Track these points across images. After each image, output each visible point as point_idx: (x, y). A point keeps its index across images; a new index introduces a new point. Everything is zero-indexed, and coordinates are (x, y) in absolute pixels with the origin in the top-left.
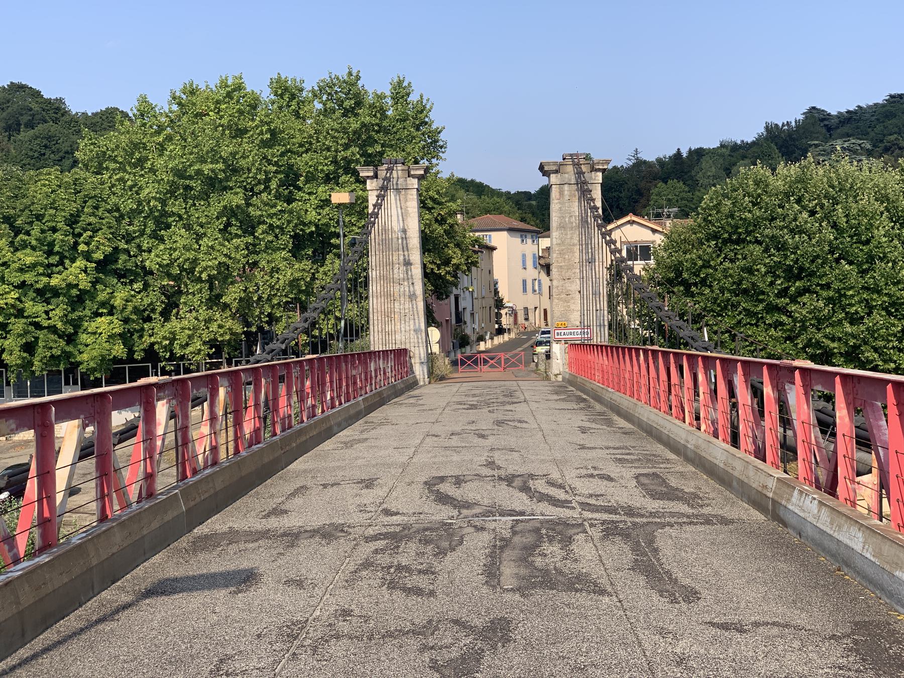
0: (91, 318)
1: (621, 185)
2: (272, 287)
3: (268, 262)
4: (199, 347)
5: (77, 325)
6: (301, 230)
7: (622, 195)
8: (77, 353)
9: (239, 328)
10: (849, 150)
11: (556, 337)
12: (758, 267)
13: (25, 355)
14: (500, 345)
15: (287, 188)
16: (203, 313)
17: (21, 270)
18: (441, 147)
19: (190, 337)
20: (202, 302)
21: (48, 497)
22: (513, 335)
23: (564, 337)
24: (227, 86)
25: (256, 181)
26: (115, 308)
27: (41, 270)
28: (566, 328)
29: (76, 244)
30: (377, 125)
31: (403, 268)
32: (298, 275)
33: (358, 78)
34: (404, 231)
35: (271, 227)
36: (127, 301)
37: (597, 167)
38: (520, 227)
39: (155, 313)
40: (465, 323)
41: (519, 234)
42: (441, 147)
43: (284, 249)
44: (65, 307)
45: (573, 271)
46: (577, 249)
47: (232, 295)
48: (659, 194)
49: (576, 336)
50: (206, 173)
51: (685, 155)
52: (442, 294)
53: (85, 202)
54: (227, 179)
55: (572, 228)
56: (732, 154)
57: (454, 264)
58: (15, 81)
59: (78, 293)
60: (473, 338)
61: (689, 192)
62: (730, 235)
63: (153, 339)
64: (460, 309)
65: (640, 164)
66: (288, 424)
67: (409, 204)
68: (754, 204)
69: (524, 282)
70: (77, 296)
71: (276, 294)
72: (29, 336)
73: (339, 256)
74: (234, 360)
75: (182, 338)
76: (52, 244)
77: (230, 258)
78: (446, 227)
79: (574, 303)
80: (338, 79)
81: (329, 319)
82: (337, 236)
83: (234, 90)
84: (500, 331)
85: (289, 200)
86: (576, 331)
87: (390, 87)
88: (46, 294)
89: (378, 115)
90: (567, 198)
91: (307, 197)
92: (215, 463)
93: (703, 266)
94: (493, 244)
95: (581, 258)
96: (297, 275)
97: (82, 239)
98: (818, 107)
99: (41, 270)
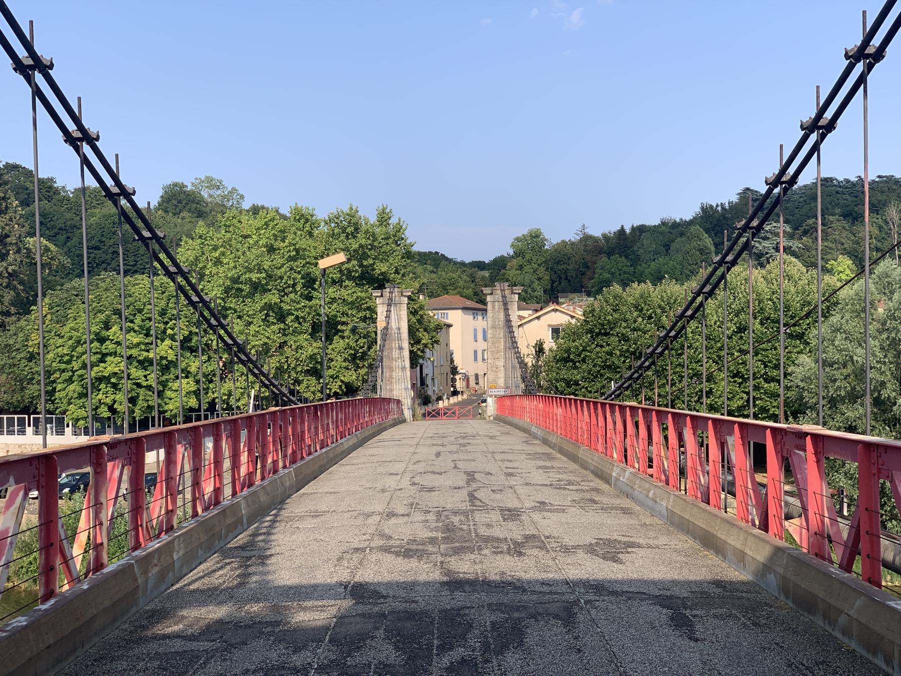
0: (174, 380)
1: (569, 259)
2: (297, 359)
3: (295, 341)
5: (164, 384)
6: (317, 319)
7: (570, 267)
8: (163, 404)
10: (771, 233)
13: (130, 405)
14: (455, 404)
15: (307, 290)
17: (128, 347)
19: (242, 394)
21: (218, 475)
22: (465, 397)
26: (190, 373)
27: (143, 347)
28: (495, 388)
30: (370, 244)
31: (398, 351)
32: (316, 351)
34: (399, 329)
35: (297, 318)
36: (199, 368)
39: (215, 377)
40: (427, 386)
41: (471, 312)
43: (305, 333)
46: (502, 341)
48: (602, 268)
51: (628, 231)
53: (169, 300)
54: (267, 284)
56: (671, 231)
57: (423, 344)
58: (11, 162)
60: (434, 398)
61: (631, 266)
62: (600, 330)
63: (216, 395)
65: (586, 238)
66: (249, 482)
67: (402, 312)
68: (614, 311)
69: (476, 352)
70: (166, 365)
72: (133, 392)
73: (343, 338)
76: (149, 329)
78: (418, 317)
80: (342, 212)
81: (336, 382)
82: (344, 323)
83: (270, 221)
84: (455, 393)
85: (310, 298)
87: (377, 212)
88: (145, 364)
89: (371, 238)
92: (170, 529)
93: (583, 350)
94: (449, 321)
95: (505, 345)
97: (169, 325)
98: (752, 188)
99: (143, 347)
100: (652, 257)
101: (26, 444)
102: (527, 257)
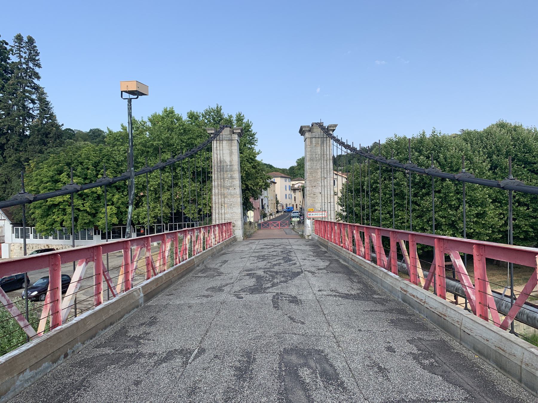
9: (167, 211)
11: (308, 216)
14: (278, 217)
16: (152, 205)
18: (256, 141)
22: (282, 213)
23: (312, 216)
24: (167, 111)
25: (176, 150)
28: (313, 212)
29: (97, 174)
33: (221, 110)
37: (330, 129)
40: (265, 209)
41: (284, 179)
42: (256, 141)
43: (188, 178)
44: (91, 202)
45: (317, 182)
47: (165, 197)
49: (319, 216)
50: (155, 145)
51: (335, 157)
52: (255, 197)
55: (317, 160)
59: (97, 196)
60: (268, 214)
62: (387, 168)
64: (263, 204)
67: (233, 148)
69: (286, 195)
75: (142, 215)
76: (86, 175)
77: (164, 181)
79: (317, 199)
80: (213, 109)
84: (278, 212)
86: (318, 213)
90: (314, 145)
91: (199, 156)
94: (275, 181)
96: (193, 189)
101: (30, 244)
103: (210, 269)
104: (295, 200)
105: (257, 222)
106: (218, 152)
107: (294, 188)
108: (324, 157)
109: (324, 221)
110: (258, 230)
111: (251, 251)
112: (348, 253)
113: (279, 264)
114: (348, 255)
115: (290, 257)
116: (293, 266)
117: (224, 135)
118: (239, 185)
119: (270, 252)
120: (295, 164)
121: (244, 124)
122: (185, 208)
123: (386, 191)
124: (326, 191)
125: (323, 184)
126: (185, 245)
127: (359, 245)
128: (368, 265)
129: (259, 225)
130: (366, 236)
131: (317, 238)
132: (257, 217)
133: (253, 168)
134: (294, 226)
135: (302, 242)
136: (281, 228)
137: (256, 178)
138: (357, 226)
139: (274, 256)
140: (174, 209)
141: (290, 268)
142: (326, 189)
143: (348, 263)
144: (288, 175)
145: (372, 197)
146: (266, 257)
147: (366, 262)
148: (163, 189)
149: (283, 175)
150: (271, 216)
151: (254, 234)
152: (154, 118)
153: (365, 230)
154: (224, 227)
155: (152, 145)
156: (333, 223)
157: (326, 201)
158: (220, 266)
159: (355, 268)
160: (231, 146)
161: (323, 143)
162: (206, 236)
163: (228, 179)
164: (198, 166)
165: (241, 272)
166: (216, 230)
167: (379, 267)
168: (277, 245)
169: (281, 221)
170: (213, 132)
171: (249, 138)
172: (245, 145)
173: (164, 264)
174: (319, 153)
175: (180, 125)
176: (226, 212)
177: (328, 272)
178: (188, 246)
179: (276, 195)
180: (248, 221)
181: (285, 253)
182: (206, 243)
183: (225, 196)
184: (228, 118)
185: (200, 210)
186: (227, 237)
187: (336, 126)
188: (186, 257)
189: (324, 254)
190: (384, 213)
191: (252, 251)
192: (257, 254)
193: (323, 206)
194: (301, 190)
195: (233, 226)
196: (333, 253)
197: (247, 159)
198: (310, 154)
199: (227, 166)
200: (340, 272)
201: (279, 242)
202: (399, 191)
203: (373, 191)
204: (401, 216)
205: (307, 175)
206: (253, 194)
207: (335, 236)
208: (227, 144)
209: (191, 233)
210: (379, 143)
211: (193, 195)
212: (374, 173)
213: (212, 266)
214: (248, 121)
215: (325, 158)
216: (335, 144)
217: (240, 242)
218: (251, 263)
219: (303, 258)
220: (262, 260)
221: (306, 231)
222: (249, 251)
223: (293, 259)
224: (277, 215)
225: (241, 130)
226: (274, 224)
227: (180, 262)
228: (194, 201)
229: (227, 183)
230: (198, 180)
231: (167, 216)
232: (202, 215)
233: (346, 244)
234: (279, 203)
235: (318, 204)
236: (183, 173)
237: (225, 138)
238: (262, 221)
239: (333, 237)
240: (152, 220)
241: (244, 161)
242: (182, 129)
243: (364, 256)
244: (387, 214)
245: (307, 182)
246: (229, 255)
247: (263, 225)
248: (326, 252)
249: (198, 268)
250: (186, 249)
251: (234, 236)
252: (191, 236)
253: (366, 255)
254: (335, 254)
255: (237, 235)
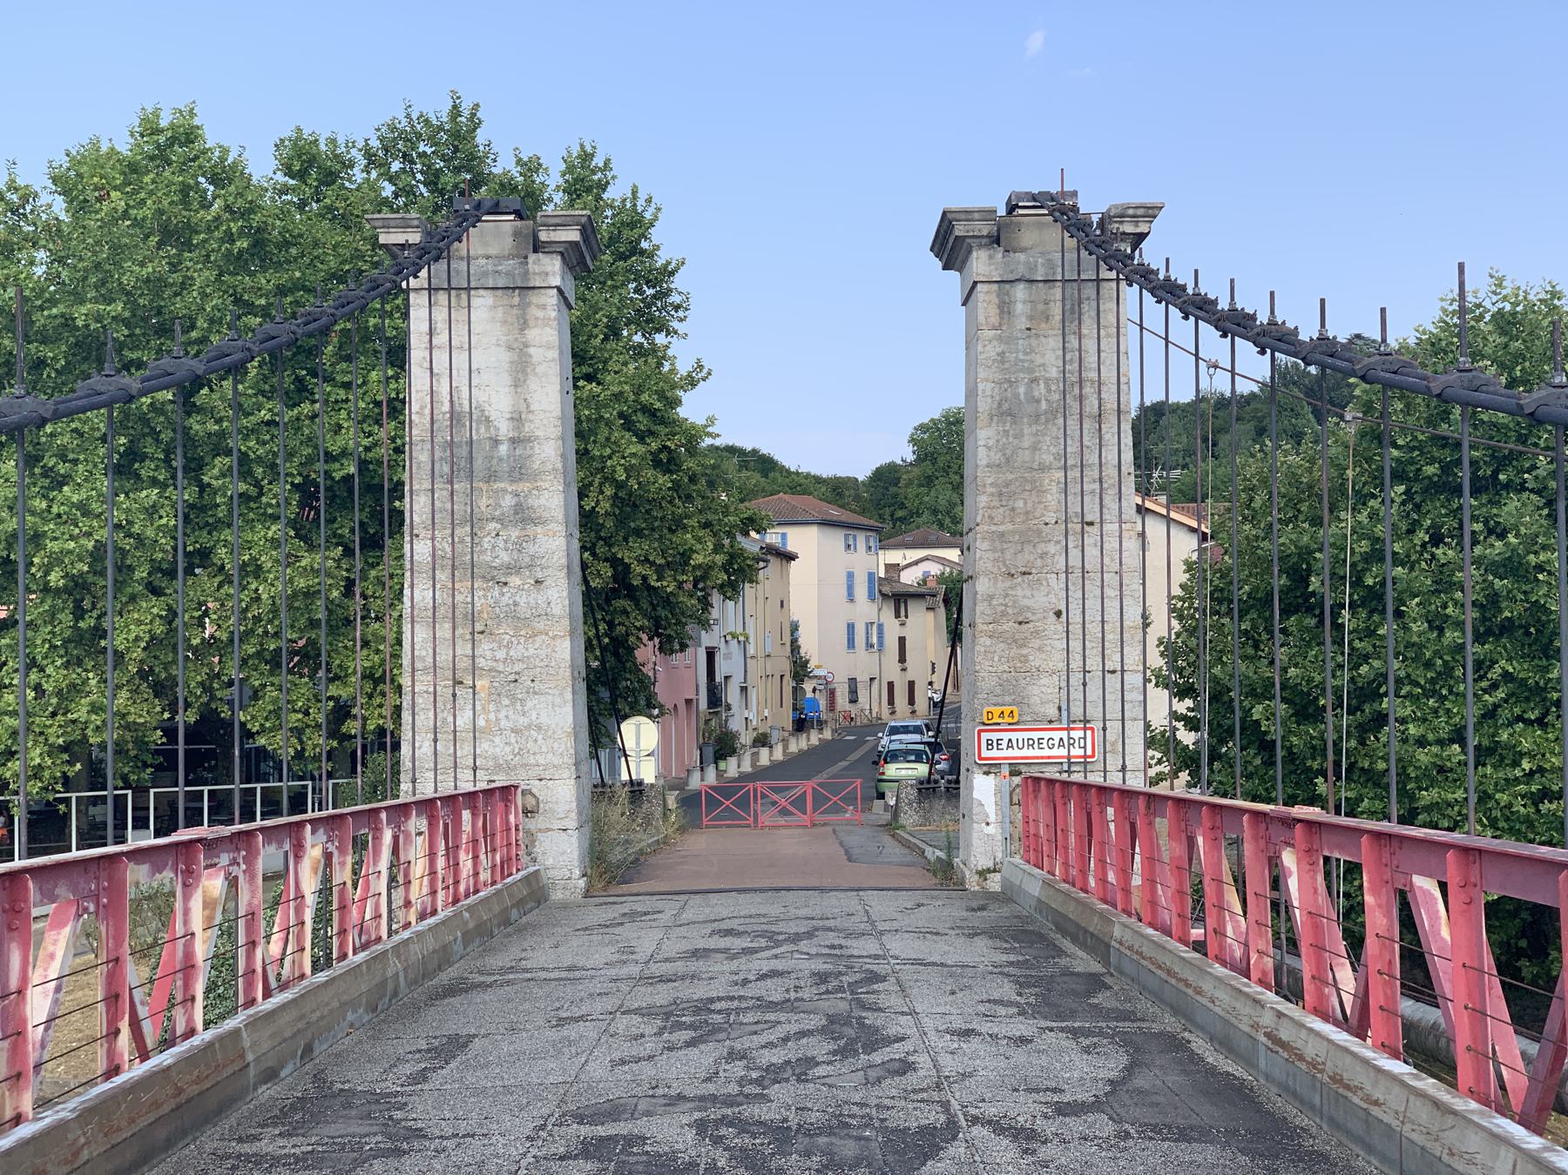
4: (38, 761)
9: (146, 713)
11: (985, 753)
12: (1543, 557)
14: (802, 754)
16: (55, 675)
18: (677, 308)
20: (53, 647)
23: (1010, 753)
24: (160, 131)
28: (1013, 727)
33: (475, 124)
38: (843, 518)
40: (729, 708)
42: (677, 308)
43: (275, 518)
45: (1041, 548)
49: (1047, 752)
50: (80, 323)
52: (670, 639)
55: (1038, 416)
60: (746, 738)
67: (533, 334)
69: (851, 628)
71: (252, 631)
74: (152, 791)
77: (129, 535)
79: (1040, 649)
80: (427, 121)
84: (801, 725)
86: (1046, 735)
90: (1022, 323)
91: (342, 394)
94: (791, 548)
96: (301, 583)
98: (1365, 335)
100: (1181, 461)
102: (941, 461)
103: (347, 1098)
104: (902, 659)
105: (680, 785)
106: (441, 358)
107: (898, 589)
108: (1081, 398)
109: (1084, 787)
110: (682, 830)
111: (624, 971)
112: (1247, 995)
113: (802, 1069)
114: (1245, 1009)
115: (870, 1018)
116: (892, 1086)
117: (483, 261)
118: (564, 561)
119: (745, 982)
120: (903, 453)
121: (609, 213)
122: (256, 695)
123: (1445, 606)
124: (1093, 604)
125: (1075, 560)
126: (180, 944)
127: (1319, 948)
128: (1397, 1089)
129: (690, 802)
130: (1375, 893)
131: (1034, 889)
132: (680, 754)
133: (657, 463)
134: (896, 811)
135: (943, 910)
136: (819, 818)
137: (678, 525)
138: (1309, 824)
139: (773, 1006)
140: (187, 705)
141: (874, 1095)
142: (1093, 590)
143: (1249, 1062)
144: (863, 512)
145: (1357, 644)
146: (718, 1018)
147: (1379, 1070)
148: (119, 586)
149: (835, 513)
150: (764, 752)
151: (652, 860)
152: (84, 169)
153: (1365, 853)
154: (466, 815)
155: (68, 322)
156: (1141, 802)
157: (1094, 663)
158: (422, 1077)
159: (1302, 1102)
160: (524, 325)
161: (1072, 314)
162: (342, 875)
163: (499, 520)
164: (335, 449)
165: (543, 1127)
166: (407, 835)
167: (1474, 1105)
168: (793, 928)
169: (822, 777)
170: (415, 238)
171: (638, 290)
172: (617, 334)
173: (19, 1076)
174: (1054, 373)
175: (228, 208)
176: (481, 722)
177: (1127, 1135)
178: (202, 950)
179: (795, 628)
180: (625, 777)
181: (841, 989)
182: (342, 921)
183: (479, 627)
184: (515, 171)
185: (342, 712)
186: (485, 876)
187: (1150, 212)
188: (190, 1020)
189: (1090, 993)
190: (1430, 737)
191: (634, 970)
192: (662, 996)
193: (1077, 695)
194: (940, 598)
195: (526, 812)
196: (1144, 989)
197: (621, 415)
198: (998, 376)
199: (496, 442)
200: (1200, 1134)
201: (803, 912)
202: (1519, 608)
203: (1363, 605)
204: (1531, 756)
205: (979, 504)
206: (657, 625)
207: (1150, 881)
208: (500, 313)
209: (234, 862)
210: (1384, 340)
211: (302, 622)
212: (1372, 503)
213: (361, 1078)
214: (634, 192)
215: (1091, 405)
216: (1154, 311)
217: (564, 906)
218: (617, 1055)
219: (958, 1024)
220: (686, 1035)
221: (969, 845)
222: (613, 972)
223: (892, 1031)
224: (799, 744)
225: (583, 232)
226: (776, 797)
227: (267, 994)
228: (309, 657)
229: (495, 549)
230: (335, 535)
231: (141, 743)
232: (359, 741)
233: (1230, 932)
234: (807, 675)
235: (1044, 681)
236: (242, 487)
237: (485, 274)
238: (711, 777)
239: (1137, 881)
240: (55, 768)
241: (608, 424)
242: (241, 233)
243: (1354, 1022)
244: (1452, 741)
245: (982, 547)
246: (488, 996)
247: (713, 803)
248: (1095, 983)
249: (266, 1092)
250: (189, 967)
251: (531, 869)
252: (233, 883)
253: (1375, 1017)
254: (1158, 998)
255: (550, 862)
